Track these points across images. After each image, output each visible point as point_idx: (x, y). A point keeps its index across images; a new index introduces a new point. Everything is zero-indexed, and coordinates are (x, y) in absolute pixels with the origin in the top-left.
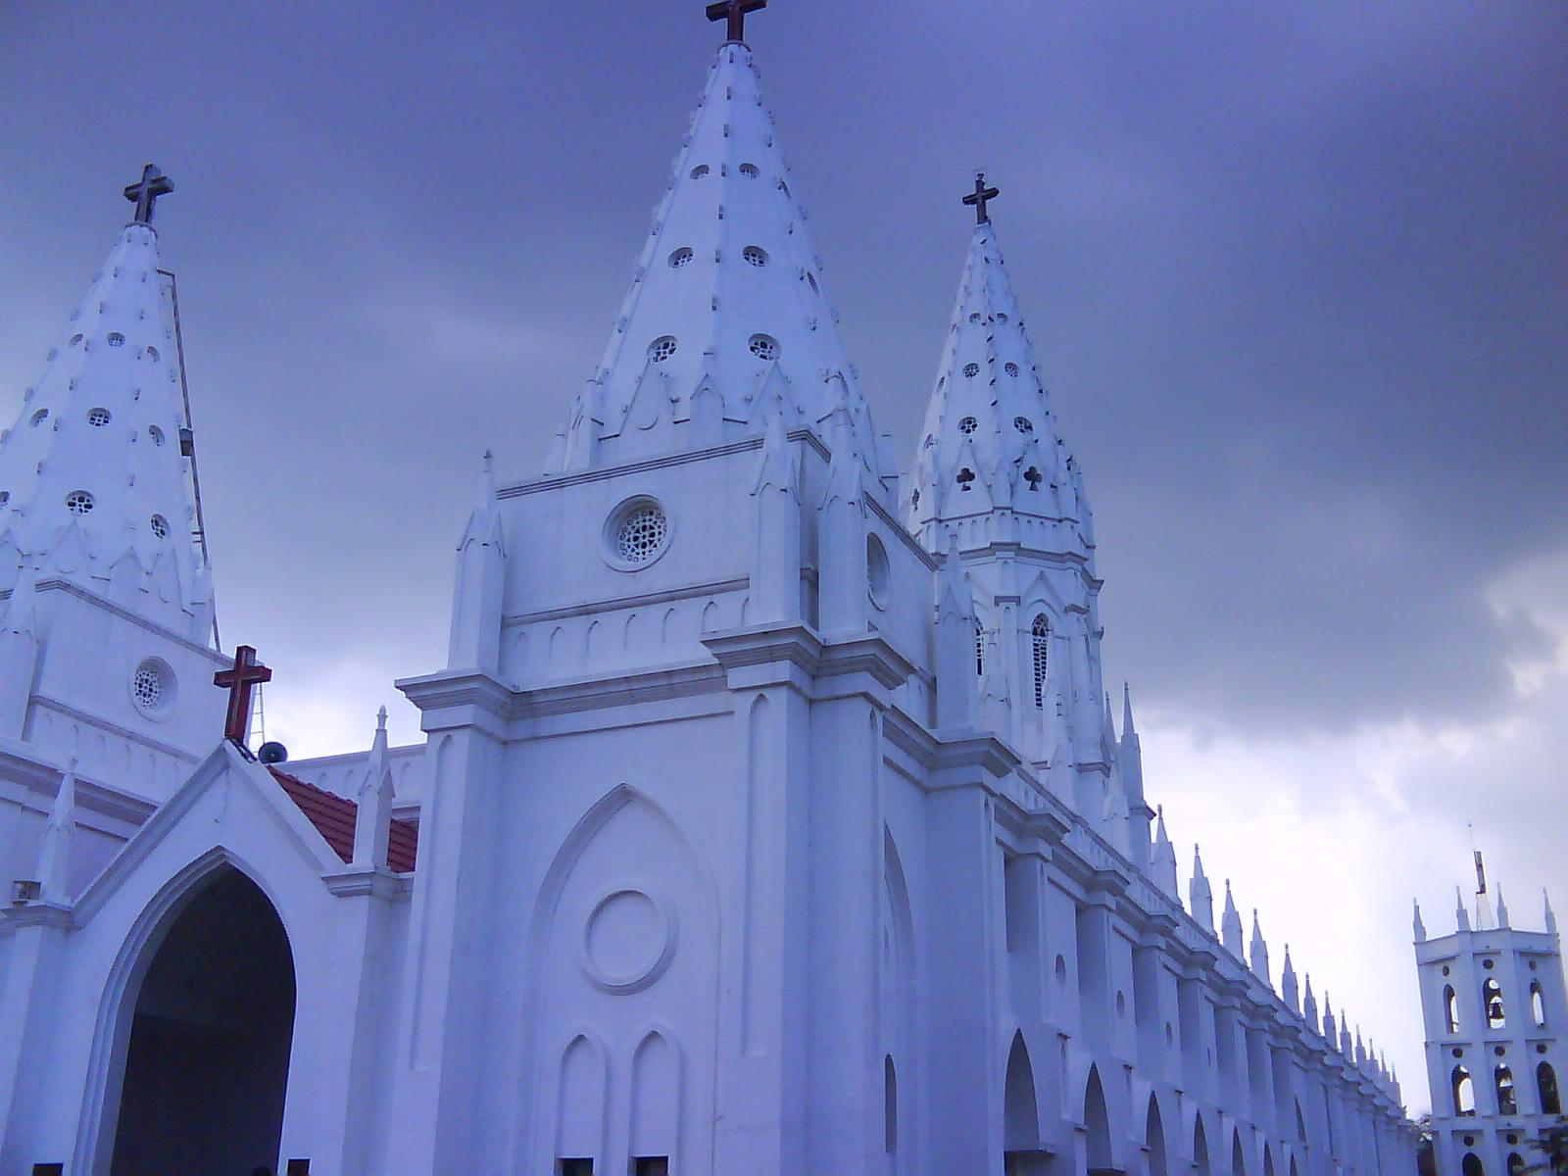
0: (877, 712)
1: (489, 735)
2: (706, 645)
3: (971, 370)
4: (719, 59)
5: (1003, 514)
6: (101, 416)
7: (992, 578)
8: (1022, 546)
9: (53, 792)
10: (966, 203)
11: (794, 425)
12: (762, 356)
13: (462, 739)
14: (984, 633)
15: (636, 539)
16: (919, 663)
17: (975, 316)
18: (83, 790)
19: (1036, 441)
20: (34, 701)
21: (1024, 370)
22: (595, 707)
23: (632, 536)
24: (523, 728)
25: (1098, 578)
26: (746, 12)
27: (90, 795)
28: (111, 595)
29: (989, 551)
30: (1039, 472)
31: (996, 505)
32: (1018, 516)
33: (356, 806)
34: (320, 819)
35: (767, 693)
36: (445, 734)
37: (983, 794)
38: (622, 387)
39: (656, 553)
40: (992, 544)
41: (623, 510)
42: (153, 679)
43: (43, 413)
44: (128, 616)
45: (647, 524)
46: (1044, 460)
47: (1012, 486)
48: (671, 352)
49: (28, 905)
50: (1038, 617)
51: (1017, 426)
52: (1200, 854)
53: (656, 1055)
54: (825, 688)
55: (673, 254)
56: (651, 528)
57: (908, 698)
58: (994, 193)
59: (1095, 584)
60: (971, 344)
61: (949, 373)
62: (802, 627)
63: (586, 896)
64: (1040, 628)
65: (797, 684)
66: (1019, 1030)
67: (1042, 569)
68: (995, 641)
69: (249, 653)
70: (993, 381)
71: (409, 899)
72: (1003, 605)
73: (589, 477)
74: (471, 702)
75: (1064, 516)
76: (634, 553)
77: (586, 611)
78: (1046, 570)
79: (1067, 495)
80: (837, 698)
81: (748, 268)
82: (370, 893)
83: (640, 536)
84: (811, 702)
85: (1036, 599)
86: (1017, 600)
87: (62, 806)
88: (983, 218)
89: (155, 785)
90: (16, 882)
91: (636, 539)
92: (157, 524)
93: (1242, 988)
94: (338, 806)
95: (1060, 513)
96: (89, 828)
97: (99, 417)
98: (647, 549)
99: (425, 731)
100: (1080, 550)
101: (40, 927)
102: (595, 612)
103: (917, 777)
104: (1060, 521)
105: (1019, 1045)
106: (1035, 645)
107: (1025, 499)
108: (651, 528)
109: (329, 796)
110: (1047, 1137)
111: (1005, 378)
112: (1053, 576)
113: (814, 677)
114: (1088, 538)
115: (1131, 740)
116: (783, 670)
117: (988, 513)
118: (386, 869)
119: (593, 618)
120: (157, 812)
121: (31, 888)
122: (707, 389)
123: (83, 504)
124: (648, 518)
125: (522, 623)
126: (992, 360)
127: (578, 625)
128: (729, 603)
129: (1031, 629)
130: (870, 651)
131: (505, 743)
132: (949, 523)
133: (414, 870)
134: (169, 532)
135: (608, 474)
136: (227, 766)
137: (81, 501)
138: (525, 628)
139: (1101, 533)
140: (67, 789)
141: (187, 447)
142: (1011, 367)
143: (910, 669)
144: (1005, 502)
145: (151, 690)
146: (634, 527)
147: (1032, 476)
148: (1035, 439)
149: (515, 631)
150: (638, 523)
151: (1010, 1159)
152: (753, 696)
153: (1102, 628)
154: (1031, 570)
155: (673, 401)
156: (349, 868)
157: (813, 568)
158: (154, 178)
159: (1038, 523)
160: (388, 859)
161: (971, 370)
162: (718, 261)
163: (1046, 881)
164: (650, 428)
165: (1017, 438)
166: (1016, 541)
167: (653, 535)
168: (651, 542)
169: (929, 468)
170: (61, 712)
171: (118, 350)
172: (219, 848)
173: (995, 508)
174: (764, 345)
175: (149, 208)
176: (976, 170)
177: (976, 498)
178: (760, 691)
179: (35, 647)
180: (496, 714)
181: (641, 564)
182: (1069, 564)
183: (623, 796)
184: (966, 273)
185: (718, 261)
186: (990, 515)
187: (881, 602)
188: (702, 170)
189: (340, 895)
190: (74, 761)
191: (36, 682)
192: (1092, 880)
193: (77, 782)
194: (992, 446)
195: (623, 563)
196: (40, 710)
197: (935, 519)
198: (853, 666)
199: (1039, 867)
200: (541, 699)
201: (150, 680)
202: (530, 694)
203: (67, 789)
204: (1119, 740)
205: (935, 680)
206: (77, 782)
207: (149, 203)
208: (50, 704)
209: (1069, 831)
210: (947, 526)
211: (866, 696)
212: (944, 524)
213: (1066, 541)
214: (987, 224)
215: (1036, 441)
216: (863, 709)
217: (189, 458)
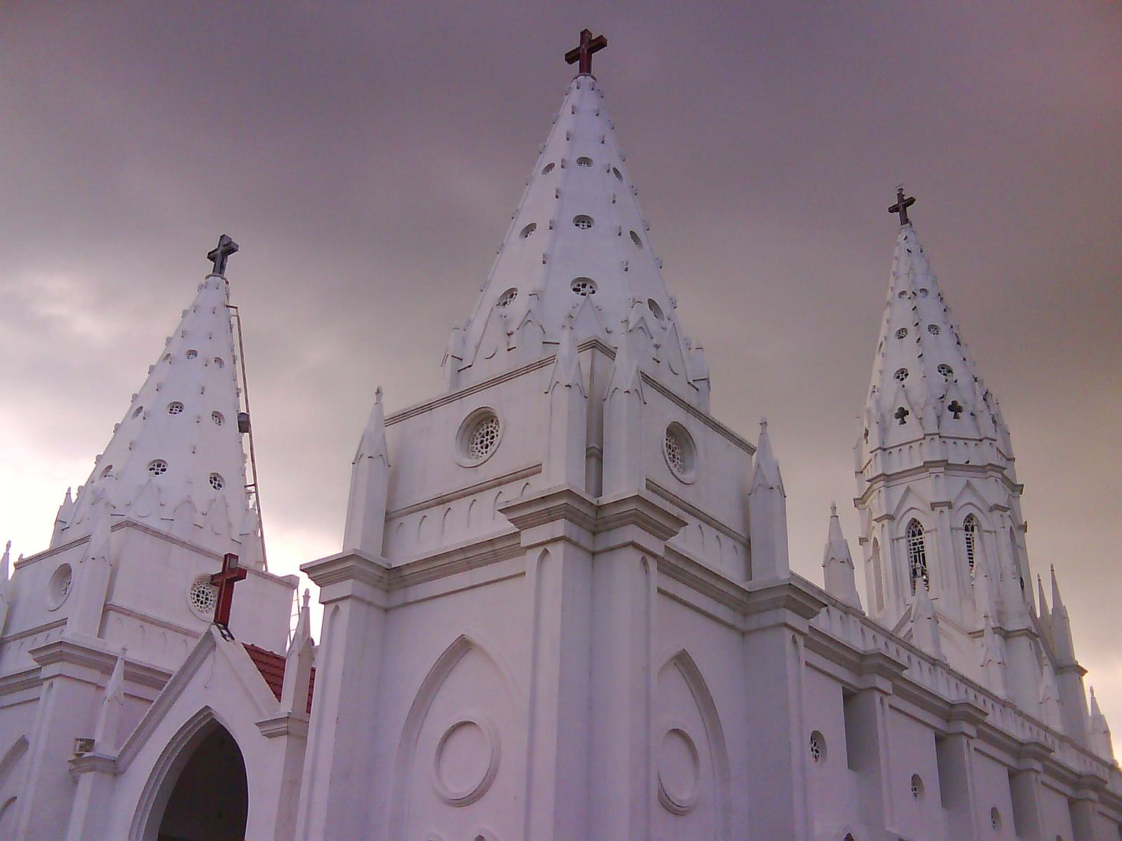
1: (370, 604)
2: (504, 513)
3: (901, 334)
4: (571, 88)
5: (932, 439)
6: (177, 407)
7: (928, 488)
8: (949, 462)
9: (108, 671)
10: (891, 211)
11: (584, 335)
13: (345, 607)
15: (482, 442)
17: (903, 293)
18: (130, 669)
19: (956, 381)
20: (107, 609)
21: (944, 329)
22: (445, 575)
23: (479, 441)
24: (398, 598)
25: (1018, 483)
26: (594, 52)
28: (176, 533)
29: (924, 469)
30: (960, 404)
32: (945, 440)
35: (549, 548)
36: (335, 604)
37: (788, 634)
40: (925, 463)
41: (472, 420)
44: (183, 544)
46: (961, 394)
49: (84, 756)
50: (968, 516)
51: (940, 371)
52: (1095, 696)
54: (603, 542)
55: (523, 230)
58: (911, 201)
59: (1017, 488)
60: (901, 314)
61: (885, 337)
62: (568, 490)
63: (436, 726)
67: (968, 478)
68: (837, 515)
69: (232, 559)
70: (919, 339)
72: (938, 509)
73: (448, 399)
74: (346, 578)
75: (982, 437)
76: (480, 454)
77: (442, 501)
78: (970, 479)
79: (985, 421)
80: (612, 549)
81: (579, 231)
82: (288, 733)
83: (485, 439)
84: (594, 554)
85: (964, 503)
86: (949, 505)
87: (115, 683)
88: (905, 220)
89: (168, 659)
90: (77, 739)
91: (482, 442)
92: (215, 480)
95: (980, 434)
97: (176, 407)
99: (322, 603)
100: (1001, 462)
101: (93, 772)
102: (449, 501)
103: (730, 621)
104: (981, 440)
106: (967, 539)
107: (951, 426)
111: (929, 337)
112: (977, 483)
113: (594, 533)
114: (1008, 454)
115: (1060, 614)
116: (559, 527)
119: (448, 505)
120: (172, 678)
121: (88, 744)
122: (530, 321)
123: (160, 468)
124: (490, 424)
125: (400, 516)
126: (917, 324)
127: (438, 511)
130: (632, 506)
132: (891, 450)
134: (225, 486)
135: (461, 395)
136: (214, 645)
137: (159, 467)
139: (1018, 447)
140: (119, 668)
142: (933, 328)
145: (207, 599)
146: (480, 434)
147: (955, 408)
148: (954, 380)
149: (395, 523)
150: (483, 430)
152: (540, 550)
153: (1026, 522)
154: (960, 480)
155: (509, 335)
157: (598, 447)
158: (225, 243)
159: (952, 443)
161: (901, 334)
162: (551, 228)
164: (493, 356)
166: (945, 459)
169: (874, 411)
170: (129, 615)
171: (194, 360)
172: (207, 707)
173: (925, 435)
175: (222, 264)
176: (897, 187)
177: (912, 429)
179: (109, 570)
180: (375, 586)
182: (991, 473)
183: (463, 646)
184: (895, 262)
185: (551, 228)
186: (923, 441)
189: (270, 736)
190: (124, 650)
194: (921, 388)
195: (468, 462)
196: (112, 615)
197: (880, 448)
198: (623, 521)
200: (407, 572)
202: (398, 569)
203: (119, 668)
204: (1051, 613)
205: (749, 541)
206: (127, 663)
207: (223, 261)
208: (120, 610)
209: (907, 668)
210: (890, 453)
211: (634, 545)
212: (888, 451)
213: (986, 455)
214: (908, 224)
215: (956, 381)
216: (633, 557)
217: (248, 434)
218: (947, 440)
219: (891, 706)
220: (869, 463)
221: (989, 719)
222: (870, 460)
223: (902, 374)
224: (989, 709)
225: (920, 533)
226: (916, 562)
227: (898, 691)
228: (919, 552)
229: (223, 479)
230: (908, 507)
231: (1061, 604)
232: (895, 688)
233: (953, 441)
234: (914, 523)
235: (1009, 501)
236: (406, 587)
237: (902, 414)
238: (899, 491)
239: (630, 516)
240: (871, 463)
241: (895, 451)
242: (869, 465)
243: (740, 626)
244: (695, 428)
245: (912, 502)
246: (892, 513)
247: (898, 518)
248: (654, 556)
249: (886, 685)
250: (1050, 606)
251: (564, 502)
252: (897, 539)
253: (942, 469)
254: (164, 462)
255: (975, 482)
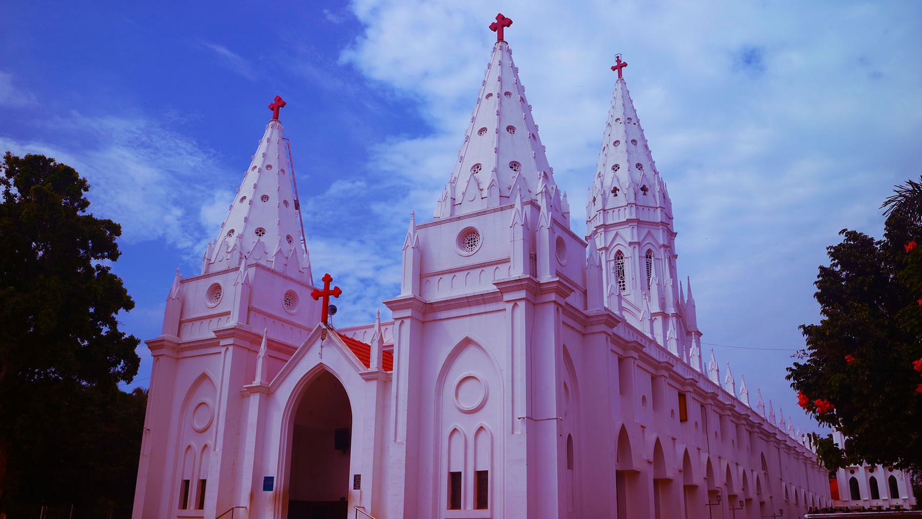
0: (559, 308)
12: (514, 170)
14: (625, 258)
16: (580, 283)
20: (249, 310)
23: (467, 242)
27: (271, 344)
31: (629, 202)
33: (370, 346)
34: (352, 346)
38: (461, 186)
39: (476, 249)
42: (290, 299)
43: (244, 198)
45: (473, 237)
47: (635, 194)
48: (480, 170)
50: (648, 250)
51: (637, 167)
53: (482, 435)
56: (474, 239)
57: (574, 300)
64: (649, 255)
65: (529, 298)
66: (623, 424)
71: (391, 381)
72: (632, 246)
73: (450, 220)
78: (650, 230)
84: (534, 304)
91: (469, 243)
93: (732, 407)
94: (362, 346)
96: (241, 347)
98: (473, 247)
103: (579, 329)
104: (657, 208)
105: (623, 431)
108: (474, 239)
109: (359, 342)
110: (637, 465)
116: (522, 294)
117: (625, 206)
118: (383, 370)
128: (503, 267)
129: (645, 256)
131: (423, 322)
132: (609, 211)
133: (392, 370)
135: (459, 218)
138: (428, 278)
141: (297, 206)
143: (576, 286)
144: (632, 201)
145: (290, 302)
147: (644, 189)
149: (425, 280)
151: (656, 481)
156: (370, 370)
160: (383, 366)
161: (616, 143)
163: (636, 366)
165: (638, 175)
167: (475, 242)
168: (474, 244)
172: (321, 363)
173: (628, 204)
174: (515, 165)
178: (515, 302)
181: (471, 253)
187: (564, 262)
188: (490, 95)
189: (367, 380)
191: (250, 303)
192: (657, 365)
193: (268, 339)
195: (464, 253)
196: (252, 313)
199: (632, 362)
201: (289, 299)
202: (432, 304)
204: (686, 302)
205: (586, 291)
206: (268, 339)
209: (645, 347)
210: (608, 212)
212: (607, 211)
213: (658, 217)
218: (639, 207)
219: (637, 365)
220: (595, 216)
221: (674, 369)
222: (597, 215)
223: (616, 168)
224: (674, 364)
225: (622, 258)
226: (619, 274)
227: (641, 358)
228: (621, 268)
229: (292, 239)
230: (616, 244)
231: (567, 202)
232: (639, 356)
233: (642, 208)
234: (619, 252)
235: (669, 243)
236: (434, 312)
237: (615, 190)
238: (611, 235)
239: (553, 289)
240: (596, 217)
241: (641, 208)
242: (595, 219)
243: (583, 331)
244: (566, 237)
245: (618, 241)
246: (607, 246)
247: (610, 250)
248: (561, 305)
249: (636, 355)
250: (686, 299)
251: (526, 282)
252: (610, 261)
253: (636, 224)
254: (263, 229)
255: (653, 231)
